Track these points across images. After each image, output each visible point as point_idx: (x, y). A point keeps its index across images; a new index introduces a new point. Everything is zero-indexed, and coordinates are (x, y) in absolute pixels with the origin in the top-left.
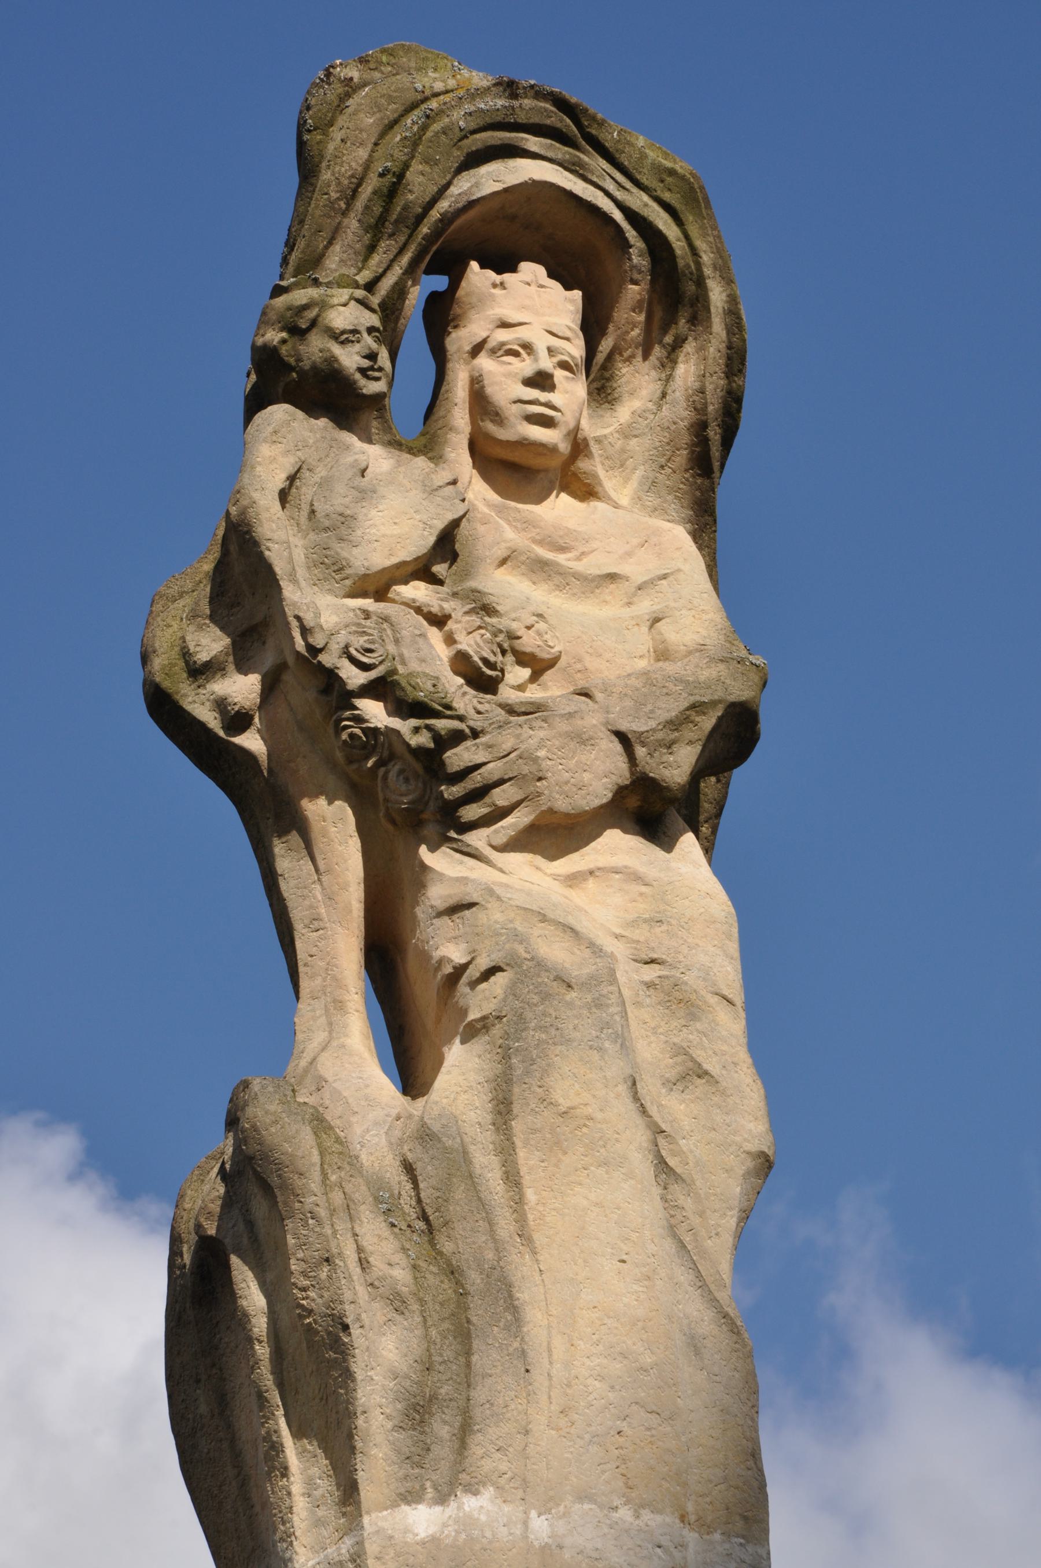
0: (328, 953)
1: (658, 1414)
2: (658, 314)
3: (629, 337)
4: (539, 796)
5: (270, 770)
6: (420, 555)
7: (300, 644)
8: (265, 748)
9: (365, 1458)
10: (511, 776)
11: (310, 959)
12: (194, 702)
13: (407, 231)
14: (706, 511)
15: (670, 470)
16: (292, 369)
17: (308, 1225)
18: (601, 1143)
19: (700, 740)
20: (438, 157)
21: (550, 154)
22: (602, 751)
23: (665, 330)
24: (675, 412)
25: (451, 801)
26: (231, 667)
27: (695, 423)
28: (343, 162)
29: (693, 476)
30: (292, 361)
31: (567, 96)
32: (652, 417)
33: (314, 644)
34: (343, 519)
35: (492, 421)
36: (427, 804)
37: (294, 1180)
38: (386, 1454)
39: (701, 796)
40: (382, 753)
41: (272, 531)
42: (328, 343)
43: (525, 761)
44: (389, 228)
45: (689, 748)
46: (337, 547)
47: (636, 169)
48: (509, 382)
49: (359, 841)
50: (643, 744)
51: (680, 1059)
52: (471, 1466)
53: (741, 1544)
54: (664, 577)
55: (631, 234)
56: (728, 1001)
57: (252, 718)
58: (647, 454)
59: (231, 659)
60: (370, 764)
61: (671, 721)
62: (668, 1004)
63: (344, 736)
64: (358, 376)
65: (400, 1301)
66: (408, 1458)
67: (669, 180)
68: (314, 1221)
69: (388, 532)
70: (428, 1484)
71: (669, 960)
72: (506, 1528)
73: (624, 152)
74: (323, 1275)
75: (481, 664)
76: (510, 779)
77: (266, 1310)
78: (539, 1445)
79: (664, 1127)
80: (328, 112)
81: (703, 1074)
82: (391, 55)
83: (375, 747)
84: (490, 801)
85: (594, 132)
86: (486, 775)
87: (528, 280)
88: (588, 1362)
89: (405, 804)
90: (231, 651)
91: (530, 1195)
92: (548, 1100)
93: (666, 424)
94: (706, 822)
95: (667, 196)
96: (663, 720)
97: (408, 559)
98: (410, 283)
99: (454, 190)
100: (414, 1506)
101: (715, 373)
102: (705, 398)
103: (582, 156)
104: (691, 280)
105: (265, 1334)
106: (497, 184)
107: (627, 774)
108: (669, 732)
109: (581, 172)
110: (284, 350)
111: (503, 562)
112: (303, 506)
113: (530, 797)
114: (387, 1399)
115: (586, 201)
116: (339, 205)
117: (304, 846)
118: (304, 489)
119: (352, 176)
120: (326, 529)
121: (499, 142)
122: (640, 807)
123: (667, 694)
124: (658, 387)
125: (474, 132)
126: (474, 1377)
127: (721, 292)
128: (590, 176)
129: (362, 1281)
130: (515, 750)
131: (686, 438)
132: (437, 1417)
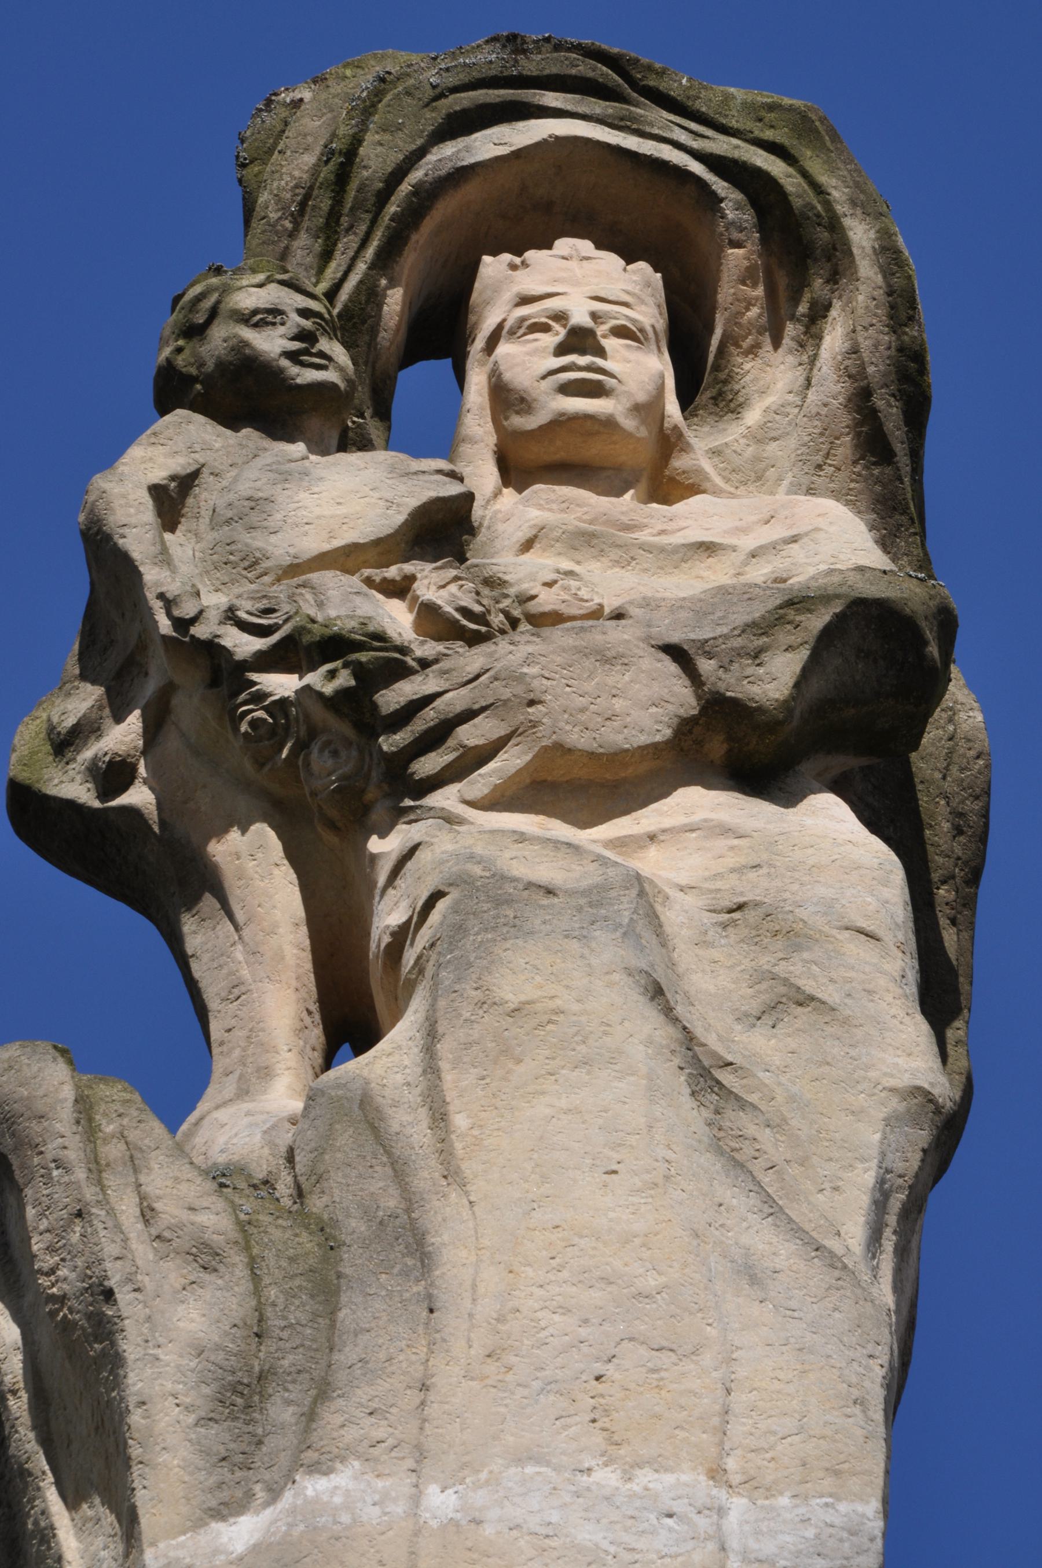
0: (251, 1019)
1: (671, 1350)
2: (782, 281)
3: (744, 320)
4: (534, 727)
5: (162, 823)
6: (382, 536)
7: (165, 625)
8: (153, 796)
9: (147, 1470)
10: (484, 704)
11: (227, 1034)
12: (62, 782)
13: (367, 217)
14: (895, 509)
15: (832, 468)
16: (194, 379)
17: (52, 1178)
18: (578, 1038)
19: (806, 643)
20: (400, 121)
21: (581, 109)
22: (643, 672)
23: (795, 299)
24: (823, 392)
25: (394, 753)
26: (109, 721)
27: (853, 394)
28: (282, 175)
29: (866, 467)
30: (193, 371)
31: (604, 46)
32: (797, 410)
33: (181, 615)
34: (253, 504)
35: (518, 413)
36: (367, 777)
37: (32, 1128)
38: (184, 1460)
39: (928, 847)
40: (298, 732)
41: (130, 516)
42: (234, 328)
43: (504, 683)
44: (345, 221)
45: (789, 655)
46: (246, 537)
47: (720, 113)
48: (535, 359)
49: (292, 871)
50: (710, 656)
51: (764, 986)
52: (321, 1440)
53: (827, 1505)
54: (794, 539)
55: (719, 185)
56: (867, 935)
57: (133, 769)
58: (793, 455)
59: (107, 711)
60: (285, 753)
61: (753, 623)
62: (758, 939)
63: (244, 727)
64: (285, 363)
65: (210, 1254)
66: (224, 1459)
67: (771, 116)
68: (60, 1170)
69: (326, 513)
70: (257, 1488)
71: (766, 900)
72: (377, 1507)
73: (699, 98)
74: (75, 1238)
75: (458, 616)
76: (484, 709)
77: (20, 1343)
78: (447, 1403)
79: (730, 1058)
80: (269, 138)
81: (805, 1000)
82: (358, 67)
83: (287, 728)
84: (455, 742)
85: (651, 83)
86: (441, 708)
87: (565, 253)
88: (540, 1292)
89: (334, 782)
90: (105, 702)
91: (460, 1121)
92: (488, 1002)
93: (814, 411)
94: (944, 882)
95: (769, 135)
96: (741, 624)
97: (362, 541)
98: (384, 282)
99: (432, 157)
100: (232, 1520)
101: (872, 325)
102: (860, 358)
103: (632, 109)
104: (819, 225)
105: (20, 1378)
106: (500, 147)
107: (693, 702)
108: (752, 638)
109: (634, 126)
110: (180, 361)
111: (528, 545)
112: (203, 513)
113: (521, 730)
114: (185, 1384)
115: (645, 155)
116: (282, 226)
117: (218, 906)
118: (204, 495)
119: (296, 186)
120: (229, 521)
121: (498, 100)
122: (729, 751)
123: (750, 599)
124: (800, 374)
125: (455, 90)
126: (340, 1337)
127: (866, 231)
128: (648, 129)
129: (145, 1237)
130: (488, 670)
131: (845, 419)
132: (277, 1399)
